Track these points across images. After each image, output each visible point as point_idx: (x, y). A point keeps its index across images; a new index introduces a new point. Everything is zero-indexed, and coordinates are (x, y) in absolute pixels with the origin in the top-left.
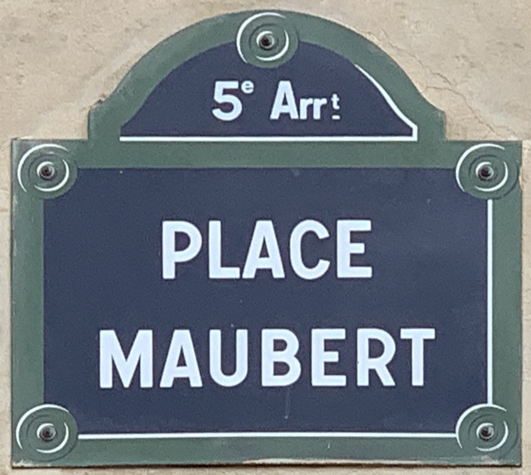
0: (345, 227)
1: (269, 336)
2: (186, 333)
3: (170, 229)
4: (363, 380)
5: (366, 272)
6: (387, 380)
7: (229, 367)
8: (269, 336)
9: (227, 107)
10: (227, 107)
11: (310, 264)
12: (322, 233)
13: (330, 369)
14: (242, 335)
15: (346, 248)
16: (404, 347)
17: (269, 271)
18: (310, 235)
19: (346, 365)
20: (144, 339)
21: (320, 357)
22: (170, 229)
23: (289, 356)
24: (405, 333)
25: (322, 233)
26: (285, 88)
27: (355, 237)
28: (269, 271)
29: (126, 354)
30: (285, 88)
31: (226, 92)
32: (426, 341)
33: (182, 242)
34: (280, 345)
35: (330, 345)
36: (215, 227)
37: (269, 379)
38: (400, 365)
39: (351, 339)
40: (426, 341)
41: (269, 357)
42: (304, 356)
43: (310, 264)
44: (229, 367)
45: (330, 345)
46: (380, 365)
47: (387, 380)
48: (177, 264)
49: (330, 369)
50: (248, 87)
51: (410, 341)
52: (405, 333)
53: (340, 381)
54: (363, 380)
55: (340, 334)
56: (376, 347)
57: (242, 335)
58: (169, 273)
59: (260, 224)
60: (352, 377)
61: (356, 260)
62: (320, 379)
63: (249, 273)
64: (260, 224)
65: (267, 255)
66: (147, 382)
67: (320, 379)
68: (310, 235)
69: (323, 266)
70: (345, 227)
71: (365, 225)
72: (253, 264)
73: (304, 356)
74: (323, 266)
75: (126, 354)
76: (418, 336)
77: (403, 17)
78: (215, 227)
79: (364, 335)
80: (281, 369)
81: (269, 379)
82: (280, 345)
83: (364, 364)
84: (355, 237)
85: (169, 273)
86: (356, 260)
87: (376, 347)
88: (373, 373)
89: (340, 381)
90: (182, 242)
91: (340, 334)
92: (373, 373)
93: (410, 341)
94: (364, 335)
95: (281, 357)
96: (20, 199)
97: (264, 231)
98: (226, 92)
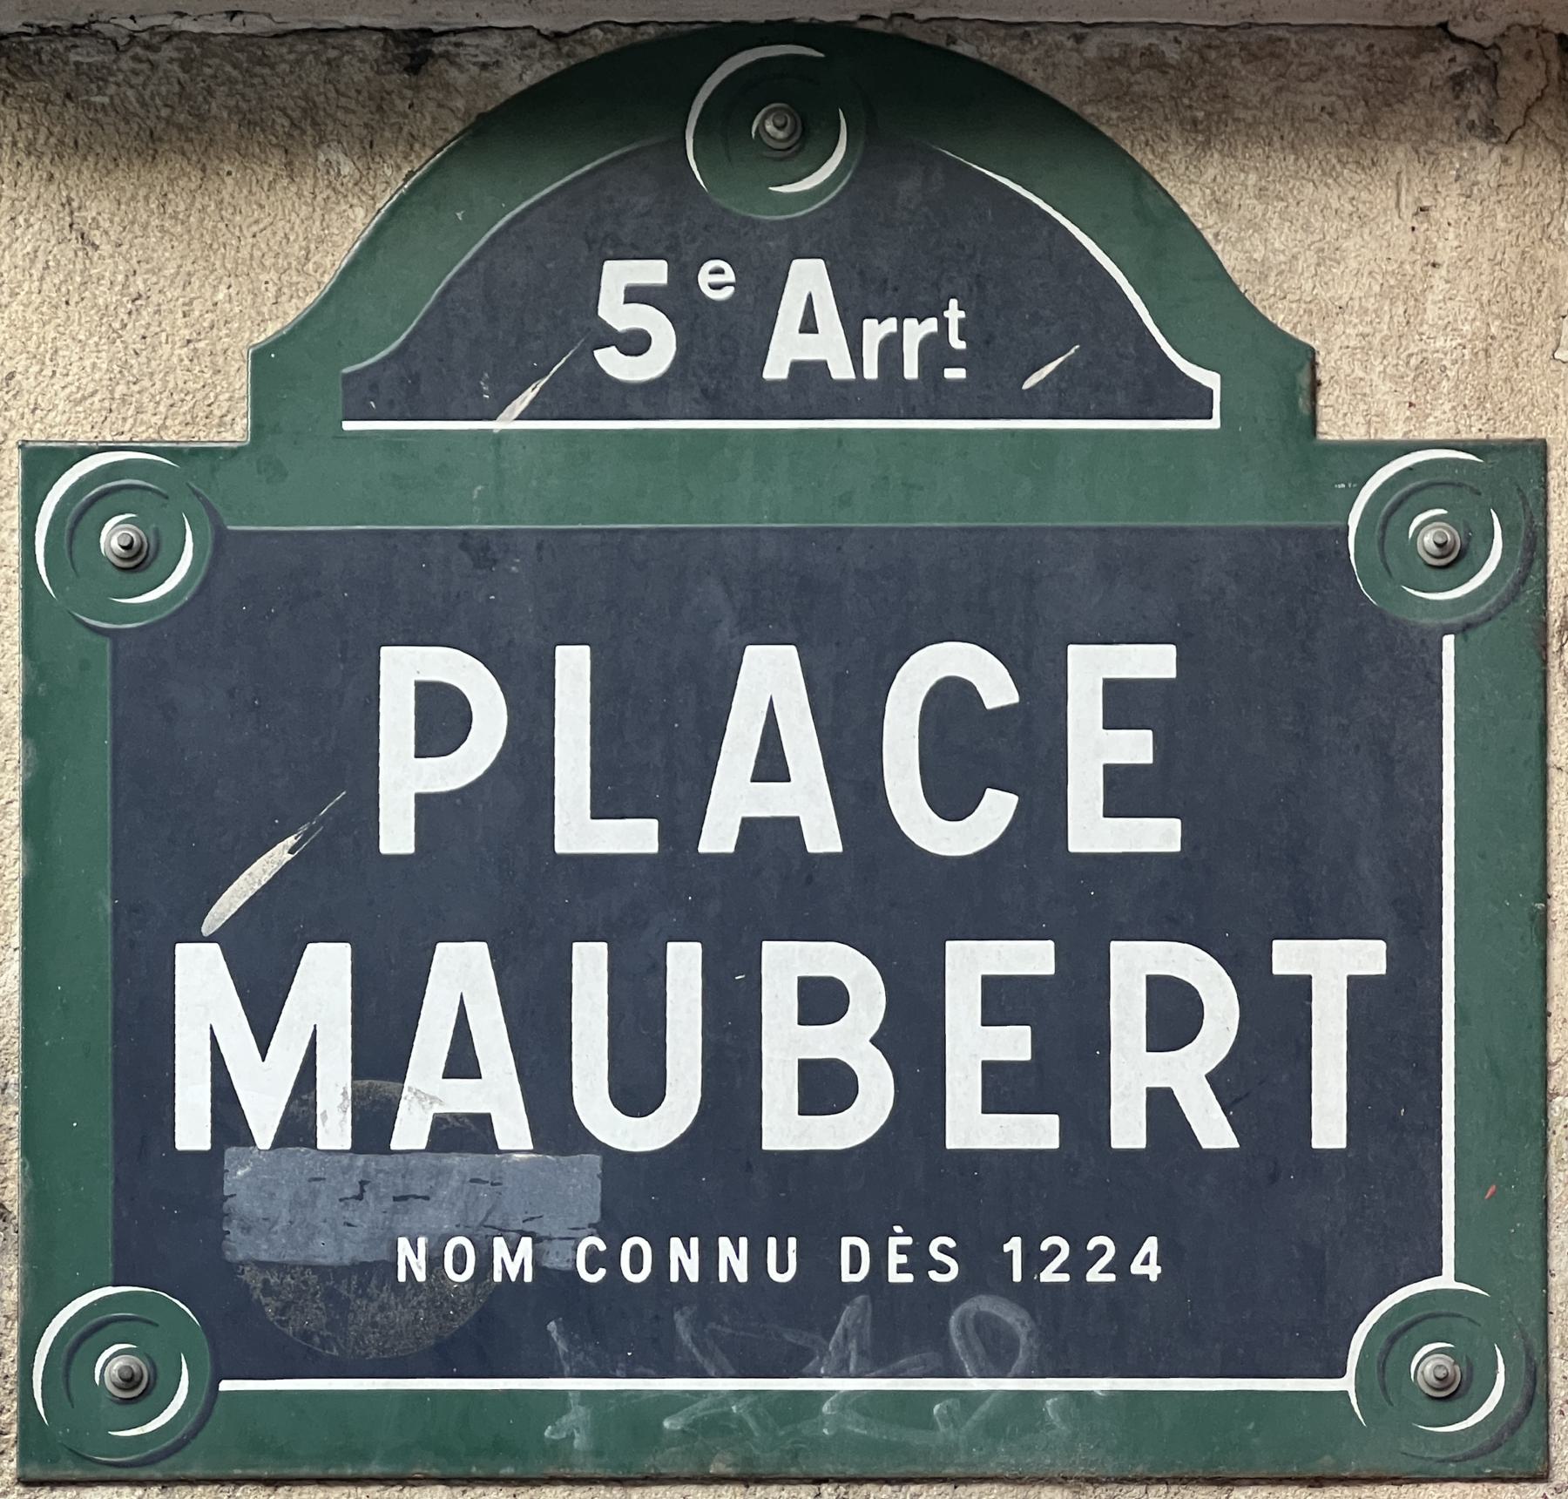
0: (1090, 668)
1: (784, 964)
2: (478, 953)
3: (403, 670)
4: (1128, 1129)
5: (1160, 835)
6: (1213, 1129)
7: (637, 1088)
8: (784, 964)
11: (952, 801)
12: (997, 687)
13: (1004, 1089)
14: (684, 964)
15: (1095, 747)
16: (1277, 1013)
18: (951, 699)
19: (1067, 1069)
20: (325, 977)
21: (973, 1044)
22: (403, 670)
23: (853, 1040)
24: (1288, 957)
25: (997, 687)
26: (808, 279)
27: (1124, 703)
29: (264, 1039)
30: (808, 279)
32: (1357, 985)
33: (442, 720)
34: (822, 1000)
35: (1001, 1002)
36: (573, 666)
37: (784, 1127)
38: (1265, 1071)
40: (1357, 985)
41: (785, 1041)
42: (913, 1039)
43: (952, 801)
44: (637, 1088)
45: (1001, 1002)
46: (1189, 1073)
47: (1213, 1129)
49: (1004, 1089)
51: (1302, 985)
52: (1288, 957)
53: (1039, 1132)
54: (1128, 1129)
55: (1034, 958)
56: (1174, 1013)
57: (684, 964)
58: (397, 835)
60: (1085, 1106)
61: (1126, 793)
62: (970, 1126)
63: (718, 836)
67: (970, 1126)
68: (951, 699)
69: (997, 811)
70: (1090, 668)
71: (1156, 662)
72: (732, 804)
73: (913, 1039)
74: (997, 811)
75: (264, 1039)
78: (573, 666)
79: (1133, 964)
80: (826, 1087)
81: (784, 1127)
82: (822, 1000)
83: (1133, 1068)
84: (1124, 703)
85: (397, 835)
86: (1126, 793)
87: (1174, 1013)
88: (1162, 1104)
89: (1039, 1132)
90: (442, 720)
91: (1034, 958)
92: (1162, 1104)
93: (1302, 985)
94: (1133, 964)
95: (824, 1042)
97: (771, 680)
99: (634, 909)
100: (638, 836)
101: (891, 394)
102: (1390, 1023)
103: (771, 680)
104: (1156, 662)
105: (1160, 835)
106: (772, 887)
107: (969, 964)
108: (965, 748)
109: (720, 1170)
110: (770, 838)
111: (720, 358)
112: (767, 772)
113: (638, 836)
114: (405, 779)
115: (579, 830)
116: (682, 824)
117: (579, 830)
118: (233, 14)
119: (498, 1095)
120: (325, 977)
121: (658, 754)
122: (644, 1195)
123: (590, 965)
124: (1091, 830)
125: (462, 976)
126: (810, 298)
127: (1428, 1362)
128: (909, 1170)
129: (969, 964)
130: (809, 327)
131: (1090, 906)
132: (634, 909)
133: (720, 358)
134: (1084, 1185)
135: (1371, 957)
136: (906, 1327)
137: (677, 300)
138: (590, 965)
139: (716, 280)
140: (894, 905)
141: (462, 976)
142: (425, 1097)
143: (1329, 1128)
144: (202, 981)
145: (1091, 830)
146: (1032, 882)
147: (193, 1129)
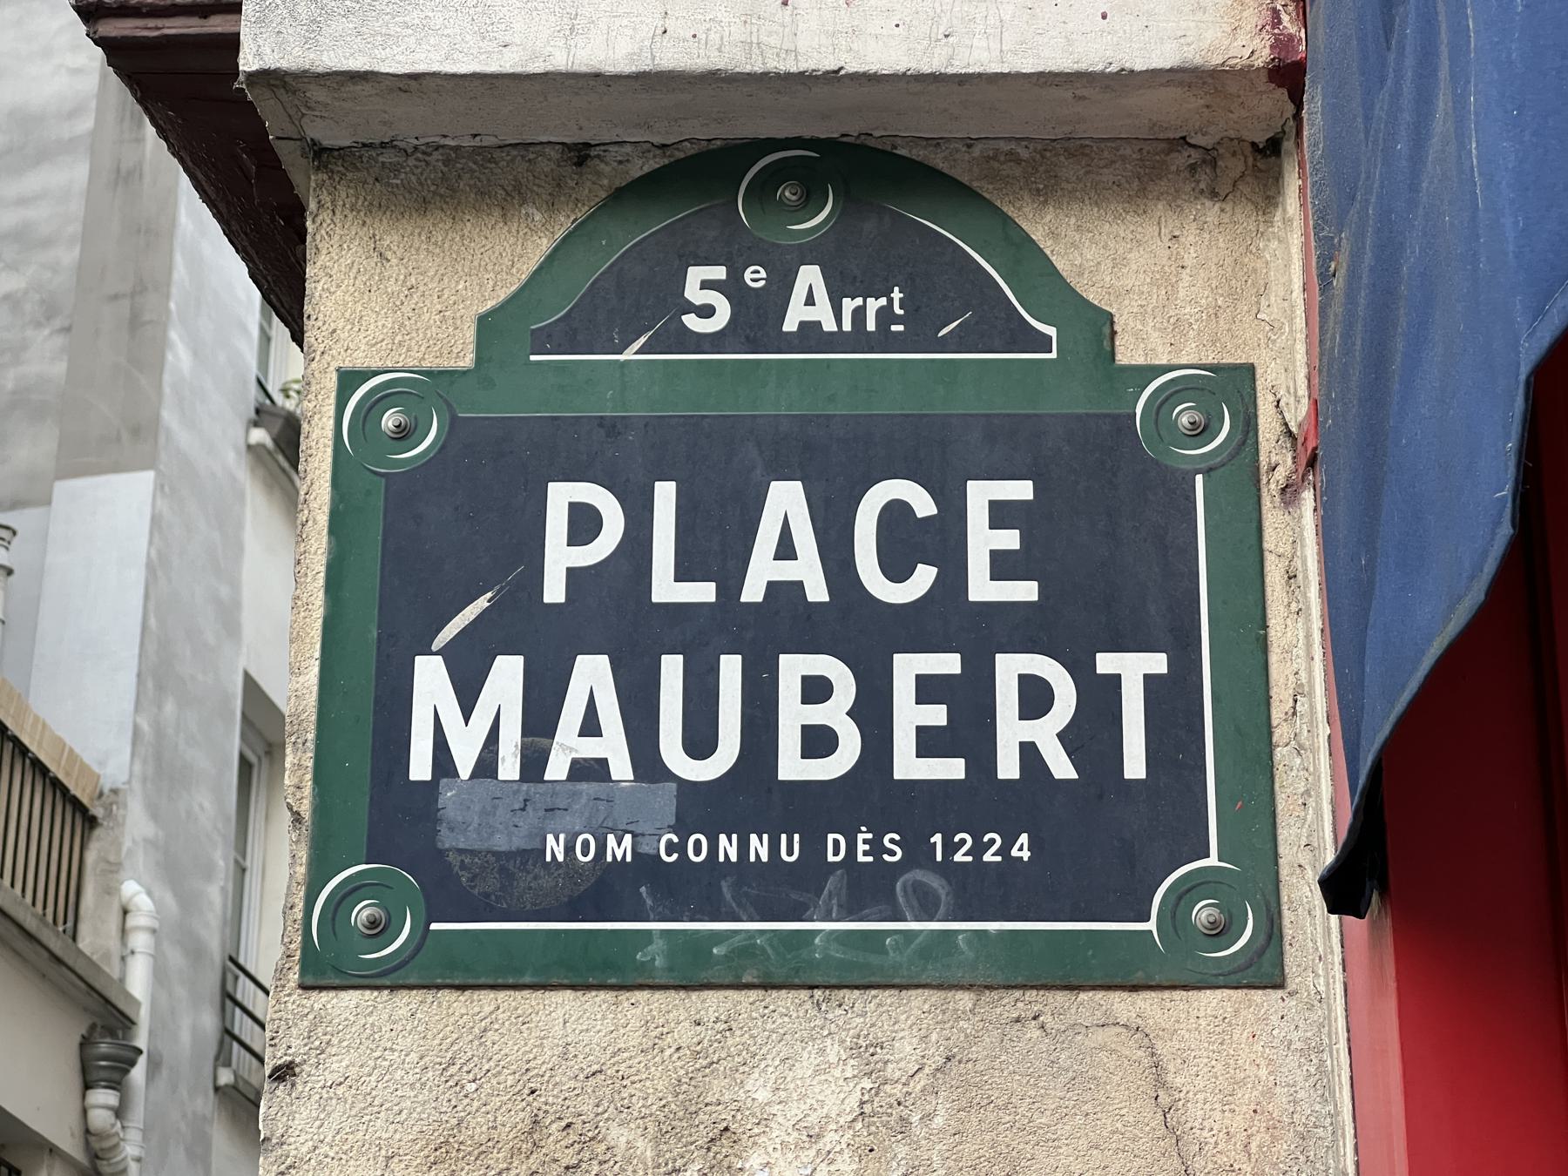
0: (980, 495)
1: (793, 668)
4: (1008, 767)
6: (1062, 767)
7: (700, 742)
8: (793, 668)
9: (707, 312)
10: (707, 312)
11: (896, 571)
12: (923, 505)
13: (929, 743)
14: (731, 668)
15: (984, 541)
16: (1100, 698)
17: (799, 586)
18: (895, 513)
19: (968, 730)
21: (910, 716)
23: (835, 713)
24: (1106, 663)
25: (923, 505)
27: (1001, 515)
28: (799, 586)
31: (706, 285)
33: (584, 524)
34: (816, 690)
35: (928, 689)
37: (792, 766)
38: (1094, 730)
42: (873, 712)
43: (896, 571)
44: (700, 742)
45: (928, 689)
46: (1046, 733)
47: (1062, 767)
48: (570, 571)
49: (929, 743)
50: (756, 276)
51: (1116, 679)
52: (1106, 663)
53: (953, 769)
54: (1008, 767)
55: (948, 664)
57: (731, 668)
58: (554, 591)
59: (776, 488)
62: (908, 765)
64: (776, 488)
65: (792, 556)
66: (509, 767)
67: (908, 765)
68: (895, 513)
69: (924, 577)
70: (980, 495)
72: (761, 574)
73: (873, 712)
74: (924, 577)
76: (1133, 670)
78: (665, 495)
80: (818, 742)
81: (792, 766)
82: (816, 690)
83: (1011, 731)
84: (1001, 515)
85: (554, 591)
87: (1035, 698)
88: (1029, 751)
89: (953, 769)
90: (584, 524)
91: (948, 664)
92: (1029, 751)
93: (1116, 679)
94: (1010, 668)
95: (817, 714)
96: (139, 289)
97: (786, 501)
98: (706, 285)
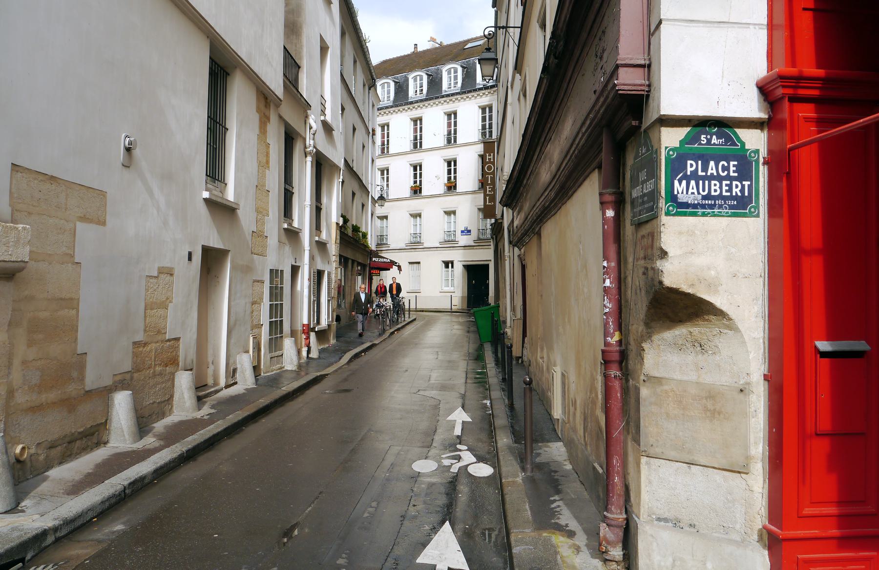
0: (732, 163)
1: (713, 182)
3: (689, 162)
4: (734, 194)
5: (736, 174)
6: (739, 194)
7: (704, 191)
12: (726, 164)
13: (727, 191)
14: (707, 182)
15: (732, 169)
16: (743, 186)
18: (723, 165)
19: (730, 190)
20: (684, 182)
21: (725, 188)
22: (689, 162)
23: (717, 188)
25: (726, 164)
26: (714, 137)
27: (734, 166)
30: (714, 137)
33: (692, 165)
34: (715, 185)
35: (726, 185)
36: (700, 162)
37: (713, 193)
38: (742, 191)
39: (731, 184)
41: (713, 188)
42: (721, 187)
44: (704, 191)
45: (726, 185)
47: (739, 194)
49: (727, 191)
52: (744, 183)
53: (729, 194)
54: (734, 194)
55: (728, 182)
57: (707, 182)
58: (689, 173)
60: (732, 193)
61: (734, 172)
67: (724, 194)
68: (723, 165)
69: (726, 173)
70: (732, 163)
71: (736, 163)
73: (721, 187)
74: (726, 173)
76: (746, 183)
77: (288, 533)
78: (700, 162)
79: (734, 183)
80: (716, 191)
81: (713, 193)
83: (734, 190)
84: (734, 166)
85: (689, 173)
86: (734, 172)
89: (729, 194)
90: (692, 165)
91: (728, 182)
94: (734, 183)
97: (712, 163)
99: (704, 178)
100: (704, 174)
101: (719, 145)
102: (750, 186)
103: (712, 163)
104: (736, 163)
105: (736, 174)
106: (712, 178)
107: (724, 183)
108: (724, 169)
109: (708, 197)
110: (712, 174)
111: (709, 141)
112: (712, 169)
113: (704, 174)
114: (689, 170)
115: (700, 173)
116: (707, 173)
117: (700, 173)
118: (190, 259)
119: (695, 191)
120: (684, 182)
121: (705, 168)
122: (704, 198)
123: (701, 182)
124: (732, 174)
125: (693, 183)
126: (410, 263)
127: (753, 210)
128: (721, 196)
129: (724, 183)
130: (714, 140)
131: (731, 179)
132: (704, 178)
133: (709, 141)
134: (731, 198)
135: (749, 183)
136: (720, 207)
137: (706, 138)
138: (701, 182)
139: (709, 137)
140: (720, 179)
141: (693, 183)
142: (690, 191)
143: (746, 194)
144: (676, 183)
145: (732, 174)
146: (728, 178)
147: (676, 193)
